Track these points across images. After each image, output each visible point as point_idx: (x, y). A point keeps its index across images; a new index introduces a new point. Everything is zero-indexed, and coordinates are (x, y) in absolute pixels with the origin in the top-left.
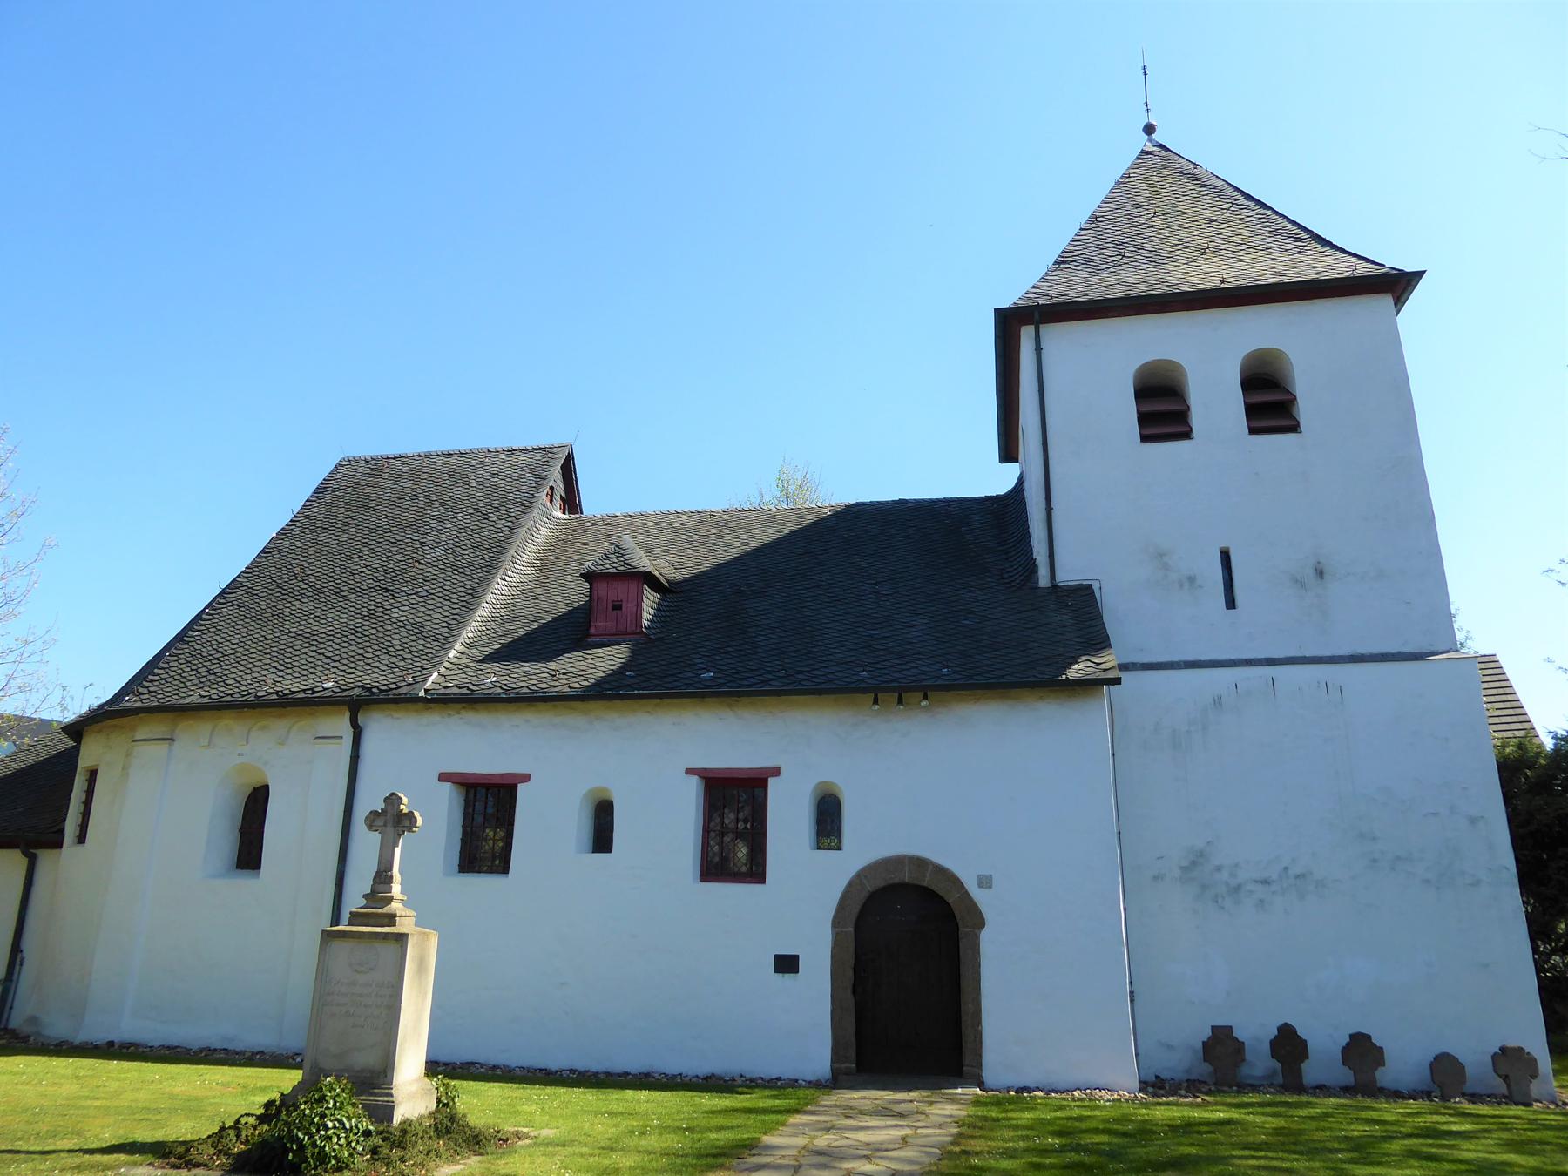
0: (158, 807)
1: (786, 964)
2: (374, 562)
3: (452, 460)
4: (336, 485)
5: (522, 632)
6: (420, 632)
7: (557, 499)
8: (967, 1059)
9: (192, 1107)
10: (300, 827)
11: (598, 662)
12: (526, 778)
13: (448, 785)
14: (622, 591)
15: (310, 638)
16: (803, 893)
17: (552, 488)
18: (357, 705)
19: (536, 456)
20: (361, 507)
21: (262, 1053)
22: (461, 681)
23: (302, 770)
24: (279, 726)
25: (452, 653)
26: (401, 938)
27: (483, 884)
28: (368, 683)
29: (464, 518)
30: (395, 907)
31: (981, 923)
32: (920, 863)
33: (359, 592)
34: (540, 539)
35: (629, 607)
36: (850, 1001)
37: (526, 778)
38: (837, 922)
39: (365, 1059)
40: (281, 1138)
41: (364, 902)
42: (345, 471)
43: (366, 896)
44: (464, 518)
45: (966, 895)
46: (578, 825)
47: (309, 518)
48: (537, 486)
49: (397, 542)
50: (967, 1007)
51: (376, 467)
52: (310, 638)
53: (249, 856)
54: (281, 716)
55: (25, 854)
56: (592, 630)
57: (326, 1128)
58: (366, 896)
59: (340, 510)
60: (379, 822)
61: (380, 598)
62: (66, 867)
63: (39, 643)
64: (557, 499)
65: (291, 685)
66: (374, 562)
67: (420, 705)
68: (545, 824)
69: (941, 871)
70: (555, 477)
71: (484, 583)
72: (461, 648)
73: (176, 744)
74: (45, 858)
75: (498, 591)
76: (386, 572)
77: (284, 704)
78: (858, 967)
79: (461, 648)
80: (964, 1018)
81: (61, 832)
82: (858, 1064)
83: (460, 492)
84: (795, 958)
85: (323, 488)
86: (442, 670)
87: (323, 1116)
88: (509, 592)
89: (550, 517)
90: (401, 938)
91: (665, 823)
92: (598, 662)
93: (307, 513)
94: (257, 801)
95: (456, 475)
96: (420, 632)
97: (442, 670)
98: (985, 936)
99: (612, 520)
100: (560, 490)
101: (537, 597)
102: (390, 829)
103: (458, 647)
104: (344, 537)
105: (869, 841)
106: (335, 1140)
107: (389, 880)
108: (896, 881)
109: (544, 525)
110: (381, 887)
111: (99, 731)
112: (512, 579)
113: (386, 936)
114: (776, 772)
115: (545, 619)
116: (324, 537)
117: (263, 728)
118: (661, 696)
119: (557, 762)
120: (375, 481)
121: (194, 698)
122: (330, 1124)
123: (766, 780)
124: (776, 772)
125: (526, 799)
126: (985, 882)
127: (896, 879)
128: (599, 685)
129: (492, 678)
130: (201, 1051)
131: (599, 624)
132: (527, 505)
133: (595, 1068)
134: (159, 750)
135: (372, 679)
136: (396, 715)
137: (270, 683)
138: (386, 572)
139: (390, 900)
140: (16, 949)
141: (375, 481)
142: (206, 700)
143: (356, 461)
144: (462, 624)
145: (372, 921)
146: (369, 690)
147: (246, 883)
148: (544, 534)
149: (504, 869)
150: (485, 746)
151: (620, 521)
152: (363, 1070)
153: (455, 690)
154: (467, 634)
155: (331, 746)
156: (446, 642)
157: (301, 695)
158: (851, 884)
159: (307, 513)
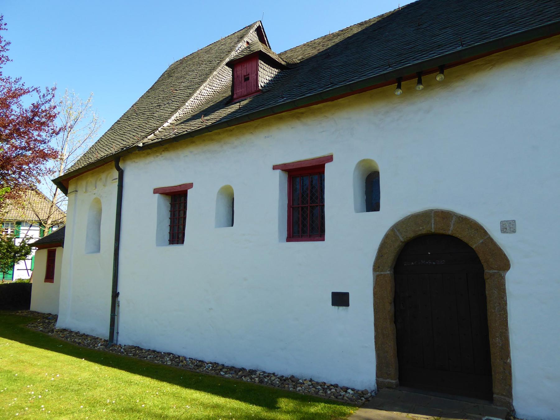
1: (340, 299)
8: (497, 388)
12: (191, 185)
13: (278, 172)
16: (354, 242)
25: (166, 125)
27: (176, 248)
31: (505, 264)
32: (445, 216)
36: (390, 328)
37: (191, 185)
38: (377, 267)
45: (489, 241)
50: (495, 341)
69: (464, 221)
73: (78, 193)
74: (58, 250)
78: (397, 300)
80: (493, 350)
82: (400, 379)
84: (334, 304)
91: (267, 201)
98: (510, 277)
105: (400, 203)
108: (424, 232)
114: (330, 159)
123: (187, 191)
124: (330, 159)
126: (508, 227)
127: (423, 230)
136: (136, 161)
140: (115, 295)
149: (182, 242)
150: (169, 170)
158: (387, 237)
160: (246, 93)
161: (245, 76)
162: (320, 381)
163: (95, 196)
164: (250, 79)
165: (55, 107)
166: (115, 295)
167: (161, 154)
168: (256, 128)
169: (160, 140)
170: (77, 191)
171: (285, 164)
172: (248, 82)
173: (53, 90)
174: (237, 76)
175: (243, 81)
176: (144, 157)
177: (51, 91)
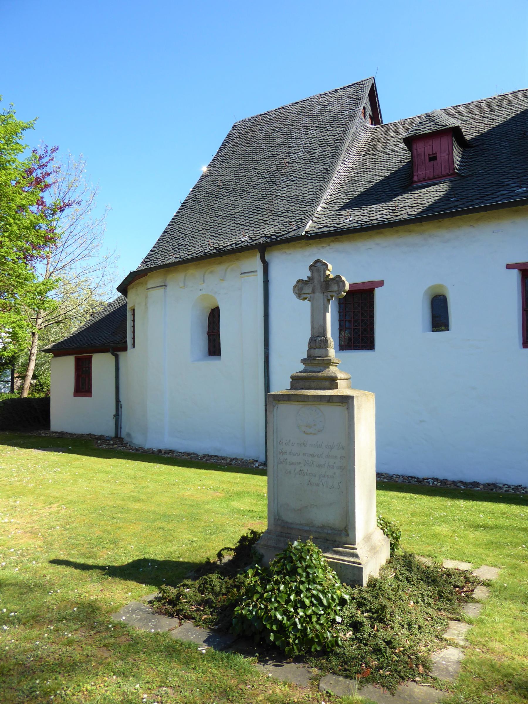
0: (165, 326)
2: (262, 169)
3: (299, 105)
4: (234, 136)
5: (362, 190)
6: (296, 200)
7: (368, 116)
9: (192, 515)
10: (239, 330)
11: (425, 197)
14: (437, 146)
15: (231, 217)
17: (364, 108)
18: (263, 248)
19: (352, 89)
20: (250, 143)
21: (236, 459)
22: (329, 223)
23: (236, 291)
24: (219, 269)
25: (319, 209)
26: (347, 401)
28: (268, 233)
29: (313, 133)
30: (333, 370)
33: (255, 187)
34: (361, 140)
35: (442, 156)
39: (325, 516)
40: (258, 618)
41: (302, 367)
42: (238, 128)
43: (304, 361)
44: (313, 133)
46: (421, 313)
47: (222, 156)
48: (356, 104)
49: (273, 156)
51: (255, 122)
52: (231, 217)
53: (214, 349)
54: (220, 263)
55: (113, 354)
56: (415, 179)
57: (304, 607)
58: (304, 361)
59: (238, 148)
60: (307, 290)
61: (268, 187)
62: (129, 358)
63: (112, 258)
64: (368, 116)
65: (222, 243)
66: (262, 169)
67: (303, 241)
68: (397, 315)
70: (366, 102)
71: (332, 165)
72: (325, 206)
73: (168, 288)
74: (122, 355)
75: (341, 170)
76: (269, 172)
77: (221, 255)
79: (325, 206)
81: (126, 342)
83: (307, 120)
85: (228, 139)
86: (315, 219)
87: (298, 593)
88: (346, 170)
89: (365, 127)
90: (347, 401)
92: (425, 197)
93: (220, 154)
94: (214, 317)
95: (303, 112)
96: (296, 200)
97: (315, 219)
99: (407, 121)
100: (369, 111)
101: (368, 170)
102: (319, 295)
103: (322, 205)
104: (242, 161)
106: (314, 619)
107: (325, 344)
109: (361, 130)
110: (317, 352)
111: (133, 288)
112: (349, 163)
113: (330, 399)
115: (377, 180)
116: (232, 163)
117: (211, 272)
118: (485, 209)
119: (399, 273)
120: (255, 128)
121: (173, 260)
122: (307, 602)
124: (381, 283)
125: (380, 296)
128: (429, 209)
129: (350, 218)
130: (204, 456)
131: (420, 173)
132: (352, 116)
133: (451, 476)
134: (160, 292)
135: (270, 231)
136: (288, 251)
137: (211, 244)
138: (269, 172)
139: (328, 363)
140: (118, 401)
141: (255, 128)
142: (179, 260)
143: (243, 121)
144: (322, 190)
145: (313, 384)
146: (270, 237)
147: (213, 363)
148: (363, 137)
150: (348, 265)
151: (413, 121)
152: (323, 527)
153: (326, 229)
154: (326, 196)
155: (251, 278)
156: (314, 202)
157: (230, 247)
159: (220, 154)
160: (432, 175)
161: (429, 155)
162: (471, 481)
163: (201, 293)
164: (438, 158)
165: (48, 174)
166: (118, 401)
167: (329, 245)
168: (478, 220)
169: (332, 228)
170: (166, 286)
171: (524, 264)
172: (435, 162)
173: (53, 151)
174: (418, 155)
175: (427, 160)
176: (301, 247)
177: (49, 152)
